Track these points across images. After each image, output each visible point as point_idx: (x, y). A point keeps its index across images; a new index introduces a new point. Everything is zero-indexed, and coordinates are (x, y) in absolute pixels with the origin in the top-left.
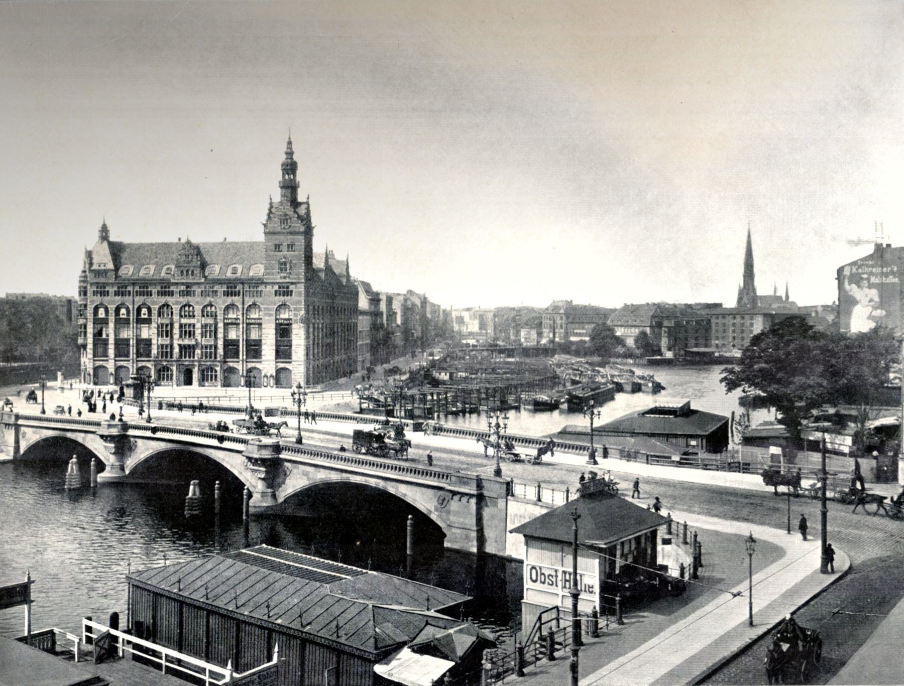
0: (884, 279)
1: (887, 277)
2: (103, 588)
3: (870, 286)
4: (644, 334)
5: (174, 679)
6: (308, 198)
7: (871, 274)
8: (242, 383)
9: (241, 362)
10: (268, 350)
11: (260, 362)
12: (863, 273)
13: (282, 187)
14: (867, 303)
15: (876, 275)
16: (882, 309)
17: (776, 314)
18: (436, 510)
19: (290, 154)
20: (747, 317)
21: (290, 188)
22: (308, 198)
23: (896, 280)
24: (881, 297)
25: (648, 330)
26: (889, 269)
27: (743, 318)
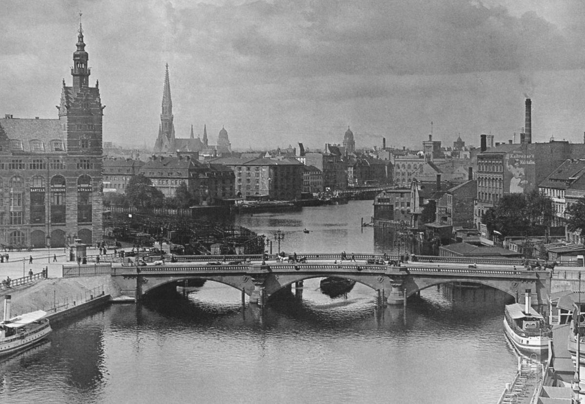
0: (527, 162)
1: (529, 161)
2: (275, 369)
3: (520, 166)
4: (183, 186)
5: (545, 344)
6: (97, 85)
7: (520, 159)
8: (48, 244)
9: (47, 226)
10: (72, 217)
11: (65, 225)
12: (516, 158)
13: (74, 75)
14: (518, 176)
15: (523, 159)
16: (526, 180)
17: (278, 165)
18: (511, 289)
19: (81, 46)
20: (252, 168)
21: (81, 74)
22: (97, 85)
23: (534, 163)
24: (526, 173)
25: (187, 182)
26: (530, 156)
27: (249, 169)
